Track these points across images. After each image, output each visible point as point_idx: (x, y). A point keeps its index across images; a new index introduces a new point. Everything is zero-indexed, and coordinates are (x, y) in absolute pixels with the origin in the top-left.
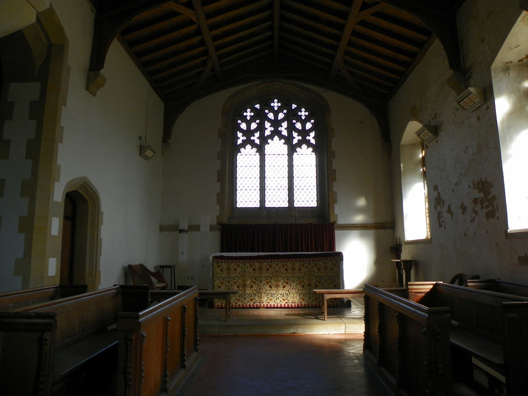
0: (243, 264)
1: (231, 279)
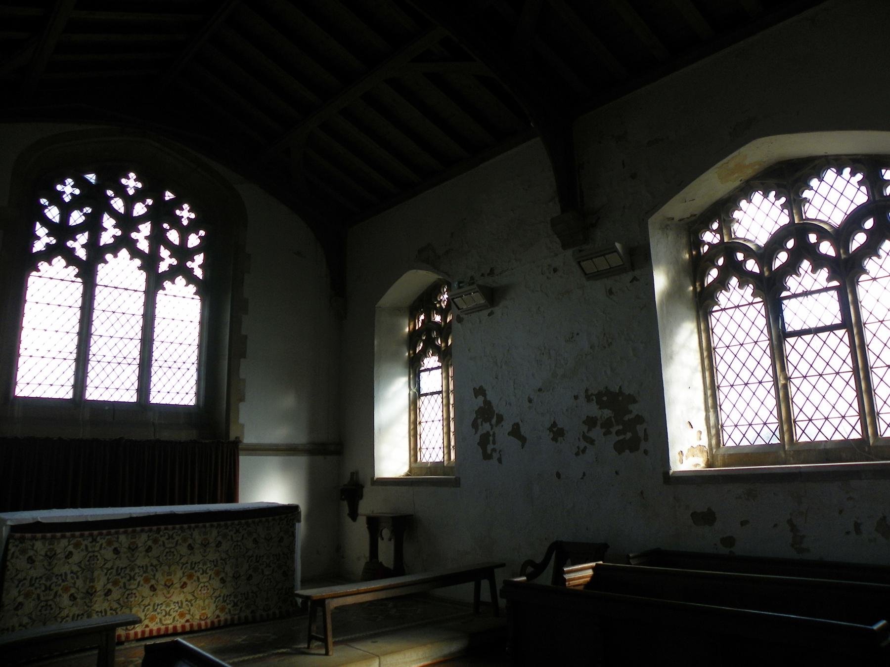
0: (90, 539)
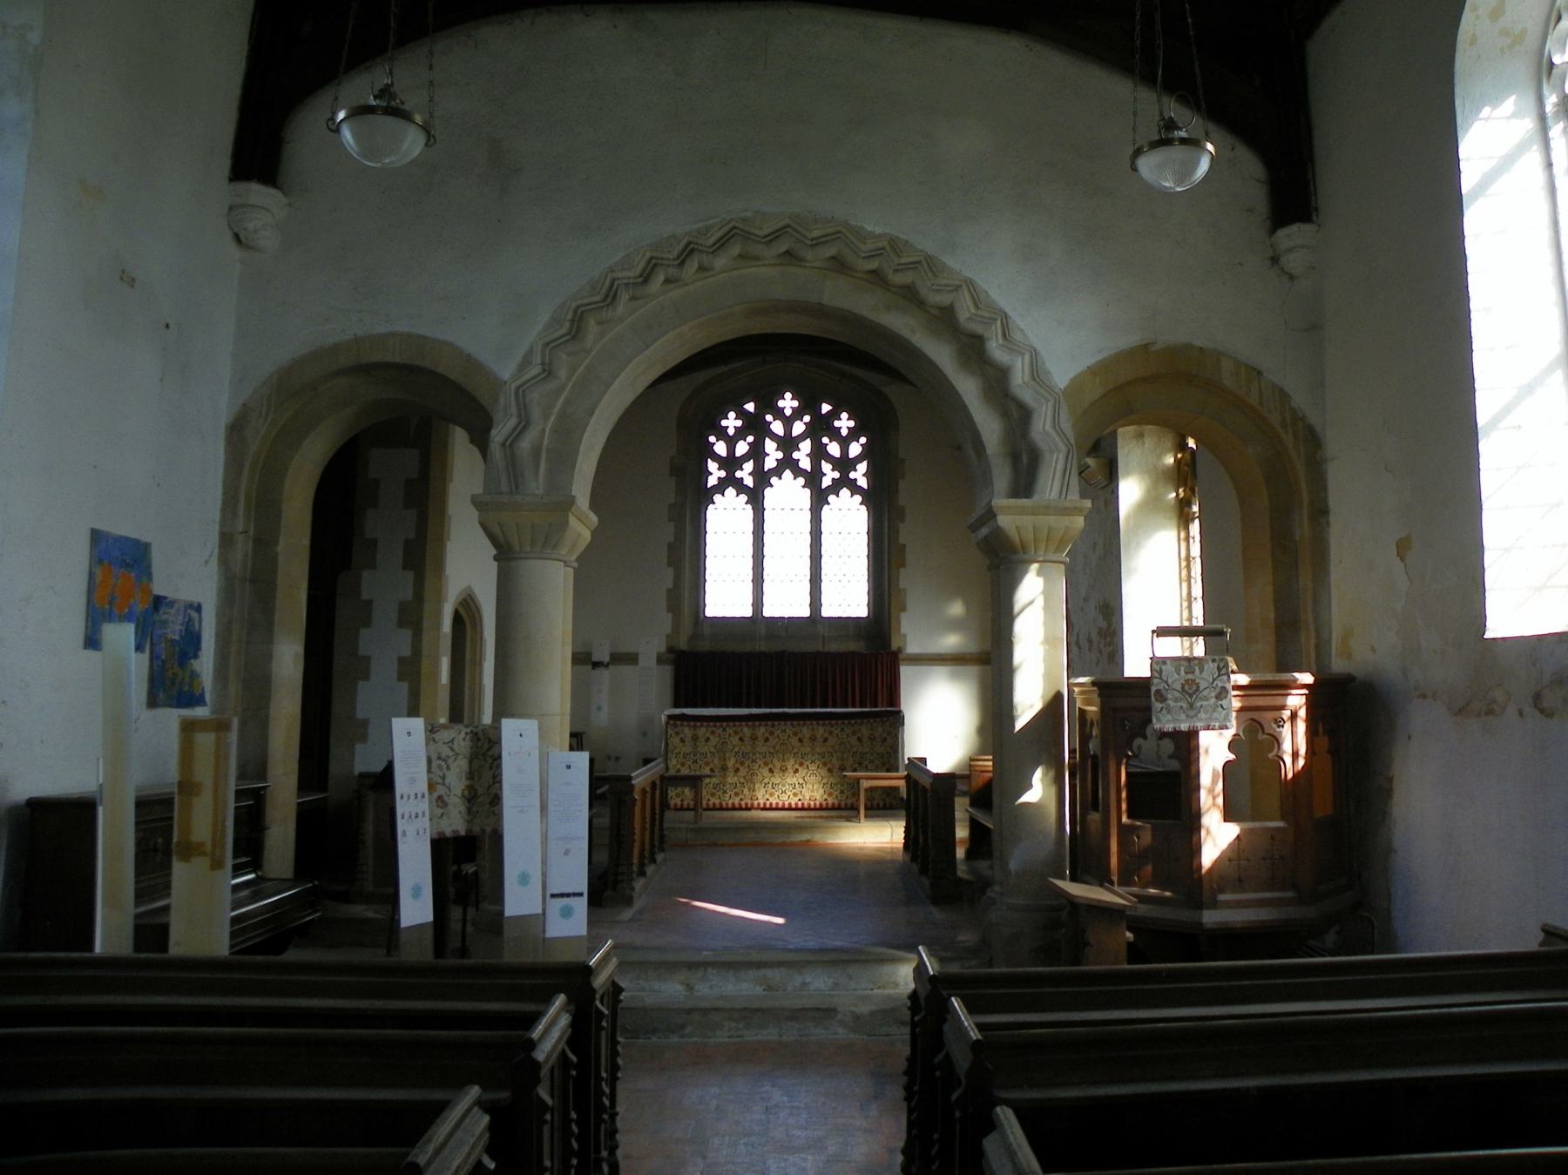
0: (721, 729)
1: (699, 756)
